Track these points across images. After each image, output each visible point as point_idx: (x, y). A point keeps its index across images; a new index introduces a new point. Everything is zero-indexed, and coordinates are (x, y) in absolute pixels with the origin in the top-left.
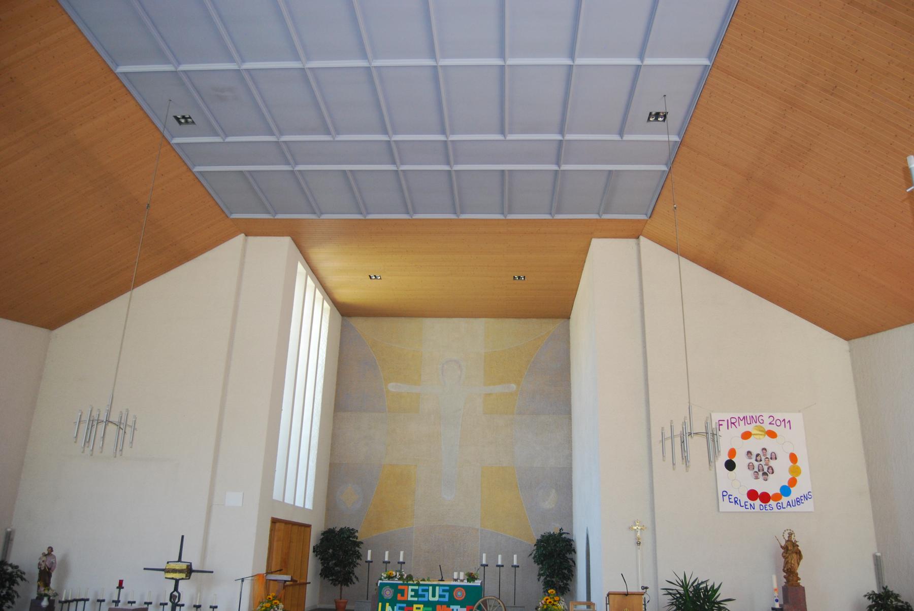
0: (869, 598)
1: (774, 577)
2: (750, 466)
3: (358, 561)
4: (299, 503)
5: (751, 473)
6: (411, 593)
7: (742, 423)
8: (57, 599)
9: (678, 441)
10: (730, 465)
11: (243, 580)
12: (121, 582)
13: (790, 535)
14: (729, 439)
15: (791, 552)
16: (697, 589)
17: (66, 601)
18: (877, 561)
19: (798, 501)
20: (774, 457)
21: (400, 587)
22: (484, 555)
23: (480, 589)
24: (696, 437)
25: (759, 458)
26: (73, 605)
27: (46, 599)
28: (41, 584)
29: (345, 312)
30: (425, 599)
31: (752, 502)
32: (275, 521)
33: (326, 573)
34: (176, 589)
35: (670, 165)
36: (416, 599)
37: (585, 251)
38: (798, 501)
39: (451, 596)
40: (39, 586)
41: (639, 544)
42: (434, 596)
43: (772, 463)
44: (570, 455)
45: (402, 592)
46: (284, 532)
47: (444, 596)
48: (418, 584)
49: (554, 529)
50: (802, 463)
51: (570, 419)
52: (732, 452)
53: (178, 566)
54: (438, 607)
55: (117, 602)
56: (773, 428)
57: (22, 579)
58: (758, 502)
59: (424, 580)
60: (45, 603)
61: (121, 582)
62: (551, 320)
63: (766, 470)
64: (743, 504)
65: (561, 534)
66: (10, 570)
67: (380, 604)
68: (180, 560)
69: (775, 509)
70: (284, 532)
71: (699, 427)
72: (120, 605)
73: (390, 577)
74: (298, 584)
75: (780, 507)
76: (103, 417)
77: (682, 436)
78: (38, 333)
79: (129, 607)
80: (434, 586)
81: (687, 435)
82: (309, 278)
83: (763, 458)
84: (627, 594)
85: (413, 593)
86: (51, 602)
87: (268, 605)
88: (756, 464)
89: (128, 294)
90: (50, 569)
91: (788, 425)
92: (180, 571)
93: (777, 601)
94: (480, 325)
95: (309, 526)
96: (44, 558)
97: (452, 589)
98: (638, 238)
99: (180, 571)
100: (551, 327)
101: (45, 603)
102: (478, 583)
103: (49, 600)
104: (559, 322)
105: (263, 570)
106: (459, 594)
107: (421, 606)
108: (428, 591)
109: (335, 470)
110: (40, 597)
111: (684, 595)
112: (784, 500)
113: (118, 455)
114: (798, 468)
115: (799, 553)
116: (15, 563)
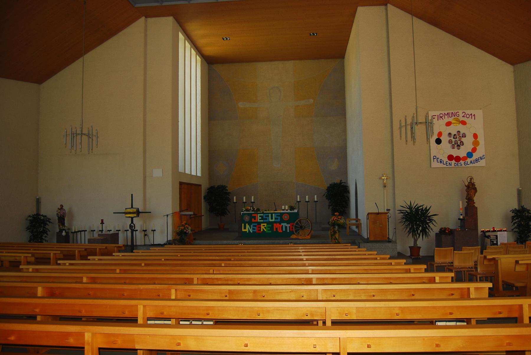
0: (513, 212)
1: (461, 202)
2: (450, 142)
3: (229, 203)
4: (194, 173)
6: (259, 218)
7: (446, 117)
8: (70, 231)
9: (409, 128)
10: (438, 141)
11: (167, 216)
12: (102, 220)
13: (471, 179)
14: (439, 126)
15: (471, 189)
16: (417, 209)
17: (75, 232)
18: (519, 192)
19: (477, 161)
20: (464, 136)
21: (253, 215)
22: (298, 196)
23: (297, 214)
24: (419, 126)
25: (455, 137)
26: (79, 234)
27: (64, 232)
29: (210, 62)
31: (450, 162)
32: (181, 184)
33: (212, 210)
34: (132, 222)
35: (372, 239)
37: (353, 15)
38: (477, 161)
39: (281, 219)
40: (59, 226)
41: (385, 186)
42: (272, 218)
43: (463, 139)
45: (255, 218)
46: (186, 189)
47: (277, 219)
48: (263, 213)
49: (337, 180)
50: (481, 139)
51: (345, 118)
52: (440, 134)
53: (131, 210)
54: (275, 225)
55: (102, 231)
56: (465, 119)
57: (50, 222)
58: (453, 162)
60: (64, 234)
61: (102, 220)
63: (459, 144)
64: (445, 163)
65: (341, 183)
66: (42, 218)
68: (132, 207)
69: (463, 166)
70: (186, 189)
71: (421, 119)
72: (104, 232)
73: (247, 210)
74: (197, 217)
76: (79, 132)
77: (412, 124)
78: (32, 86)
79: (108, 233)
80: (272, 214)
81: (414, 123)
82: (186, 42)
83: (458, 137)
84: (378, 214)
86: (67, 233)
87: (183, 228)
88: (453, 140)
89: (82, 58)
90: (63, 216)
91: (473, 117)
92: (133, 213)
93: (461, 215)
94: (290, 65)
95: (200, 185)
98: (386, 5)
99: (133, 213)
101: (64, 234)
102: (296, 211)
103: (66, 232)
105: (178, 210)
107: (266, 224)
108: (268, 216)
109: (211, 153)
110: (61, 231)
111: (410, 213)
112: (469, 160)
113: (90, 152)
114: (478, 142)
115: (475, 190)
116: (44, 214)
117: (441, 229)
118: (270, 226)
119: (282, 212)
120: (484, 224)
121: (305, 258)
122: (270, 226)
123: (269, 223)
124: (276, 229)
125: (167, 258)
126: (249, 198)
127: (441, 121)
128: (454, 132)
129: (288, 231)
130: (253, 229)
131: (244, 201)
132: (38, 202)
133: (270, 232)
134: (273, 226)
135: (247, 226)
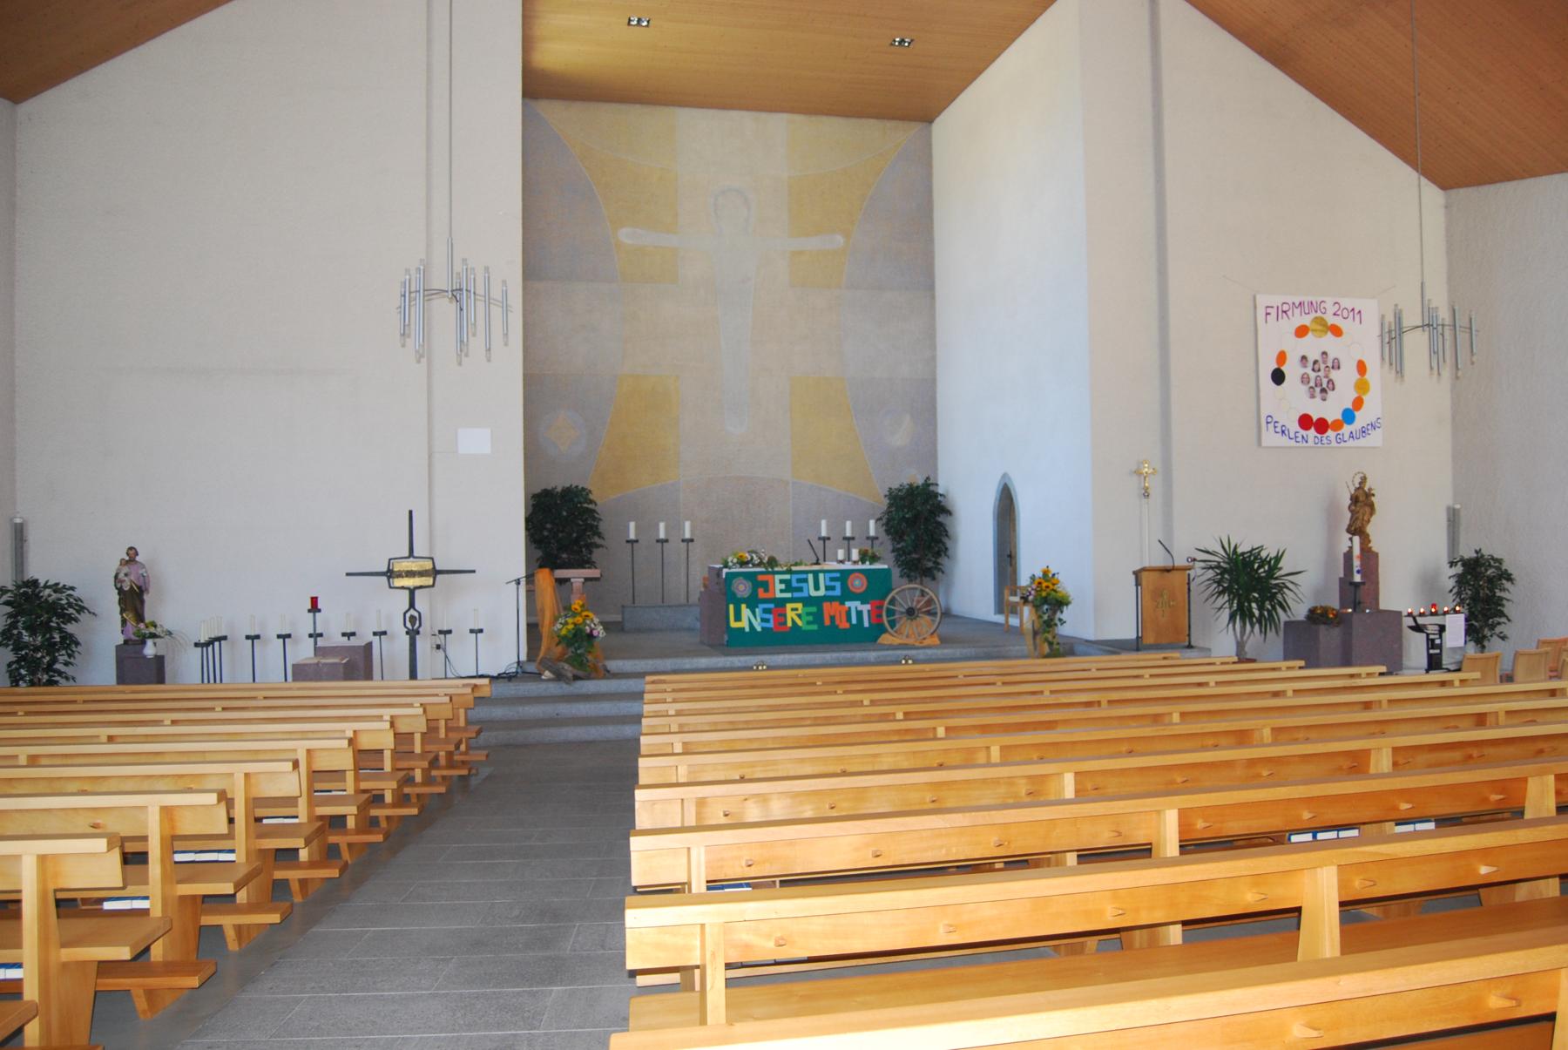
2: (1305, 379)
3: (597, 540)
5: (1305, 388)
6: (779, 586)
10: (1278, 377)
12: (314, 601)
13: (1364, 480)
18: (1453, 518)
19: (1364, 431)
20: (1336, 366)
21: (760, 578)
28: (129, 616)
30: (804, 594)
34: (412, 605)
36: (788, 595)
38: (1364, 431)
39: (844, 587)
40: (124, 622)
42: (817, 588)
43: (1334, 375)
44: (933, 359)
45: (766, 586)
47: (833, 588)
48: (789, 572)
51: (933, 297)
52: (1282, 357)
54: (826, 605)
56: (1338, 321)
57: (81, 609)
58: (1312, 432)
59: (796, 564)
61: (314, 601)
62: (900, 124)
67: (731, 607)
69: (1334, 444)
75: (1340, 440)
80: (815, 573)
85: (783, 586)
88: (1313, 375)
92: (400, 575)
94: (778, 124)
96: (125, 569)
97: (845, 574)
99: (421, 574)
100: (899, 135)
104: (915, 128)
106: (857, 583)
107: (799, 606)
108: (806, 580)
112: (1346, 429)
115: (1372, 506)
117: (1312, 611)
118: (814, 609)
119: (842, 567)
120: (1397, 593)
121: (672, 709)
122: (814, 609)
123: (808, 601)
124: (832, 619)
125: (1115, 696)
126: (675, 526)
127: (1284, 321)
128: (1313, 355)
129: (866, 624)
130: (763, 620)
131: (632, 536)
132: (19, 534)
133: (815, 627)
134: (821, 611)
135: (746, 612)
